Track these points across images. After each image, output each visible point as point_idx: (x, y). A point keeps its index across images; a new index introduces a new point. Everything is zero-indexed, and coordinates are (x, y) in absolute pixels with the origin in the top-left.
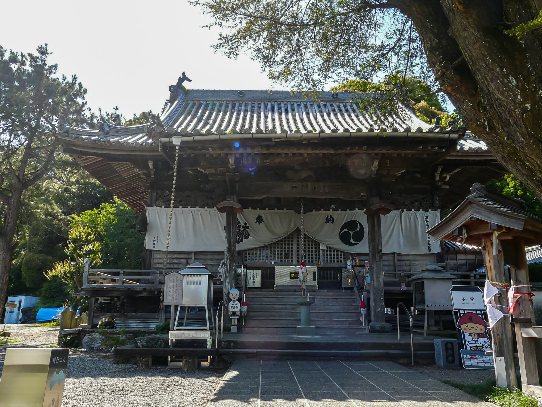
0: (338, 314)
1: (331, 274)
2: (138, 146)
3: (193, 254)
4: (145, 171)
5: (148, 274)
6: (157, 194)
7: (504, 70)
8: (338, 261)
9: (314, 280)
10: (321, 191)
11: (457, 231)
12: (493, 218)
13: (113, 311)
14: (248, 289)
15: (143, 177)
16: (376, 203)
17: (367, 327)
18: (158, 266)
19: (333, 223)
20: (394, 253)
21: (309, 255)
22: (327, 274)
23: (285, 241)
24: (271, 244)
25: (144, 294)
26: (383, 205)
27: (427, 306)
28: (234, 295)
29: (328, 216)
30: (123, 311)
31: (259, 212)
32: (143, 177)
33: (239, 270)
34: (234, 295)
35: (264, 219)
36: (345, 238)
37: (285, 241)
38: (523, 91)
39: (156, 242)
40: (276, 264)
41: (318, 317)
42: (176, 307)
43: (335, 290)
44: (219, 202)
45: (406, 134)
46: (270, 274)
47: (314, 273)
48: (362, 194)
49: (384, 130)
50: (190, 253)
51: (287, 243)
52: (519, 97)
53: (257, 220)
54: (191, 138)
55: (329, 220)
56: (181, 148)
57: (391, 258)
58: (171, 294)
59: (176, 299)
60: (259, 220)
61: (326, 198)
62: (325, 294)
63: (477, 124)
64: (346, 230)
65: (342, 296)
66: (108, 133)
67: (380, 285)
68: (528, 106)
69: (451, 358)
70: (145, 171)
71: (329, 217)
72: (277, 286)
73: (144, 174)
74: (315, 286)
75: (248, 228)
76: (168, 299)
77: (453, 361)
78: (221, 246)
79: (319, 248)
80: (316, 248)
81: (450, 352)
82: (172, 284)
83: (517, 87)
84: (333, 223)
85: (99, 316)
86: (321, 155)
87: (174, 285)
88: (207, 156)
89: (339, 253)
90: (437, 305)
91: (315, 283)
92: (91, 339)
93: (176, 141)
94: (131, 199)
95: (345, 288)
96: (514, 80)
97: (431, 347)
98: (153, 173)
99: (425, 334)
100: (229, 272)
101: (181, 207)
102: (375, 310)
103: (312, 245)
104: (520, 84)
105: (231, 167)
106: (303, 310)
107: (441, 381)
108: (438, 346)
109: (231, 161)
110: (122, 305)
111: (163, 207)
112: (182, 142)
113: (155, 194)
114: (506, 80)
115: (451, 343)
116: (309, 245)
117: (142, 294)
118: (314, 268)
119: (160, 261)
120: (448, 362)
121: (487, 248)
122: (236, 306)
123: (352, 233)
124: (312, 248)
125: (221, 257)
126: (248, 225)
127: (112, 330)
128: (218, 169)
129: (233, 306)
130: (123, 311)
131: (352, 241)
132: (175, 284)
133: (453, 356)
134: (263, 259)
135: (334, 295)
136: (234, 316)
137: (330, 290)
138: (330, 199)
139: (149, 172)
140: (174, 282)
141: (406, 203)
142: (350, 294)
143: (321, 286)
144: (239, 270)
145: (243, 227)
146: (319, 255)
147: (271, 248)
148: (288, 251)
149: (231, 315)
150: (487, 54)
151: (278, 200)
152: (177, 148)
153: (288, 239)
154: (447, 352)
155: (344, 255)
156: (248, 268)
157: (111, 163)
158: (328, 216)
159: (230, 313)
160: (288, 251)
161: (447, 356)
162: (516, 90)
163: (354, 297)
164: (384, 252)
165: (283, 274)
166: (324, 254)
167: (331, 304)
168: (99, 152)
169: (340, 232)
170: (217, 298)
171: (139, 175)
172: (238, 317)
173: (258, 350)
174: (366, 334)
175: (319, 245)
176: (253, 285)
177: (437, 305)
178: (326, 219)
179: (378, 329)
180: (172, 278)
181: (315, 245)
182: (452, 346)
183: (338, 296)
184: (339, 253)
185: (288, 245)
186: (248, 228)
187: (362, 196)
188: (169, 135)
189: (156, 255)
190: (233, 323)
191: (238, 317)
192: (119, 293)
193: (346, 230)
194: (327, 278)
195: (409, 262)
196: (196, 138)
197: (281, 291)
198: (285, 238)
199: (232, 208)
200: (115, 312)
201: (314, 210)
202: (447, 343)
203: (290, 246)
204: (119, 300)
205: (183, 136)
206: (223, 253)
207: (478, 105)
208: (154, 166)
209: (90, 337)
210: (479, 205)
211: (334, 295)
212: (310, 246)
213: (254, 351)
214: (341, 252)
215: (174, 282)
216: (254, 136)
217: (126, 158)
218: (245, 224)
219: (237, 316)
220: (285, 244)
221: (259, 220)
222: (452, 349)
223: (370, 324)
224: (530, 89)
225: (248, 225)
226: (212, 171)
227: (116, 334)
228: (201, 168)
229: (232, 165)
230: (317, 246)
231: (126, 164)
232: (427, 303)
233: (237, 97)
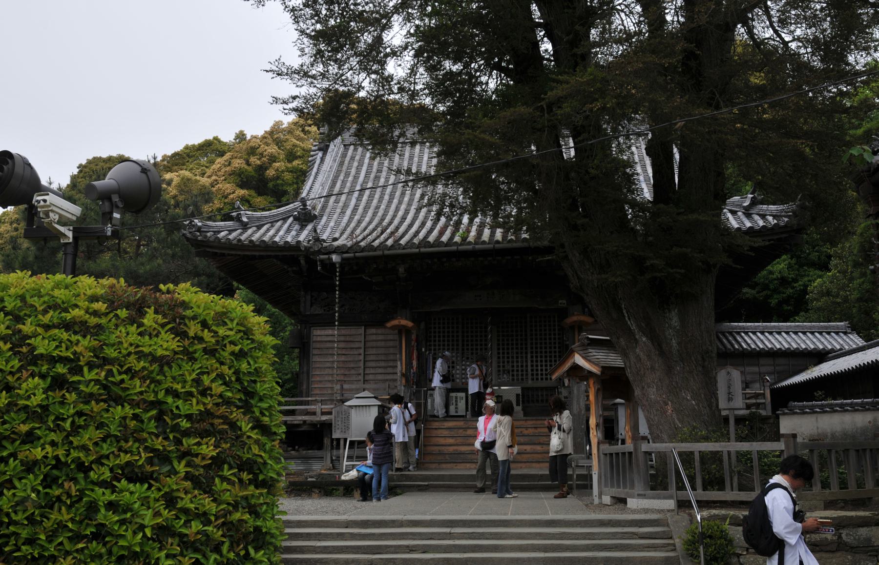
4: (295, 268)
6: (312, 297)
25: (304, 428)
47: (518, 395)
56: (341, 264)
70: (295, 268)
93: (335, 258)
109: (401, 270)
112: (343, 259)
113: (309, 297)
194: (538, 401)
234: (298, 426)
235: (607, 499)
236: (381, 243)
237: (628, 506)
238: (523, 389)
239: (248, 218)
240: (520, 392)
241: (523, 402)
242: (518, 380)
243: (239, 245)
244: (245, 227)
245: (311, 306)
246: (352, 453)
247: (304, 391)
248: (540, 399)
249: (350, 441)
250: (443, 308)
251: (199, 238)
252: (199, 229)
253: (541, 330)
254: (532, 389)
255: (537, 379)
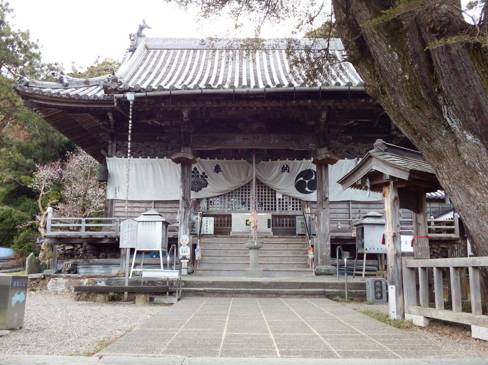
0: (288, 258)
1: (286, 221)
2: (96, 99)
3: (153, 203)
4: (105, 123)
5: (110, 222)
6: (117, 144)
7: (389, 46)
8: (297, 209)
9: (269, 227)
10: (272, 142)
11: (360, 181)
12: (388, 170)
13: (76, 257)
14: (202, 236)
15: (103, 128)
16: (323, 153)
17: (314, 270)
18: (119, 214)
19: (288, 172)
20: (349, 201)
21: (265, 203)
22: (283, 221)
23: (242, 190)
24: (229, 193)
25: (106, 241)
26: (328, 156)
27: (366, 249)
28: (184, 240)
29: (284, 166)
30: (85, 257)
31: (216, 161)
32: (103, 128)
33: (194, 218)
34: (184, 240)
35: (221, 167)
36: (300, 187)
37: (242, 190)
38: (403, 64)
39: (117, 192)
40: (232, 211)
41: (268, 261)
42: (132, 250)
43: (286, 236)
44: (173, 154)
45: (347, 88)
46: (228, 221)
47: (269, 220)
48: (311, 145)
49: (327, 85)
50: (150, 202)
51: (244, 191)
52: (400, 69)
53: (215, 170)
54: (143, 94)
55: (285, 169)
56: (135, 102)
57: (345, 206)
58: (126, 238)
59: (131, 243)
60: (217, 169)
61: (272, 149)
62: (277, 239)
63: (373, 89)
64: (301, 179)
65: (294, 241)
66: (67, 85)
67: (326, 231)
68: (407, 77)
69: (379, 295)
70: (105, 123)
71: (285, 166)
72: (233, 233)
73: (104, 125)
74: (269, 233)
75: (206, 177)
76: (124, 244)
77: (381, 297)
78: (176, 194)
79: (275, 196)
80: (272, 196)
81: (378, 289)
82: (127, 230)
83: (399, 61)
84: (288, 172)
85: (63, 262)
86: (269, 108)
87: (129, 231)
88: (162, 109)
89: (295, 201)
90: (376, 249)
91: (270, 229)
92: (56, 283)
93: (130, 97)
94: (93, 149)
95: (299, 235)
96: (397, 55)
97: (363, 286)
98: (112, 124)
99: (363, 275)
100: (184, 219)
101: (140, 157)
102: (321, 254)
103: (268, 193)
104: (401, 59)
105: (185, 120)
106: (252, 253)
107: (364, 313)
108: (368, 284)
109: (185, 114)
110: (85, 252)
111: (123, 157)
112: (136, 98)
113: (115, 145)
114: (390, 55)
115: (381, 282)
116: (265, 193)
117: (103, 241)
118: (269, 215)
119: (121, 209)
120: (377, 298)
121: (386, 195)
122: (186, 251)
123: (307, 181)
124: (269, 196)
125: (175, 205)
126: (206, 174)
127: (76, 275)
128: (174, 122)
129: (183, 250)
130: (85, 257)
131: (307, 189)
132: (130, 229)
133: (381, 292)
134: (218, 208)
135: (285, 241)
136: (184, 259)
137: (281, 236)
138: (268, 149)
139: (109, 124)
140: (129, 227)
141: (362, 152)
142: (301, 240)
143: (275, 232)
144: (194, 218)
145: (201, 176)
146: (275, 203)
147: (229, 196)
148: (246, 199)
149: (182, 259)
150: (376, 32)
151: (236, 151)
152: (131, 103)
153: (247, 187)
154: (375, 289)
155: (300, 203)
156: (203, 216)
157: (71, 114)
158: (284, 166)
159: (181, 257)
160: (246, 199)
161: (376, 293)
162: (398, 63)
163: (304, 242)
164: (331, 199)
165: (239, 221)
166: (279, 203)
167: (283, 249)
168: (59, 104)
169: (296, 180)
170: (172, 243)
171: (99, 125)
172: (188, 261)
173: (206, 289)
174: (312, 277)
175: (275, 193)
176: (207, 232)
177: (376, 249)
178: (282, 168)
179: (324, 271)
180: (127, 224)
181: (272, 193)
182: (381, 284)
183: (289, 241)
184: (295, 201)
185: (242, 193)
186: (206, 177)
187: (311, 146)
188: (124, 91)
189: (117, 204)
190: (183, 266)
191: (188, 261)
192: (81, 240)
193: (301, 179)
194: (279, 225)
195: (358, 210)
196: (148, 94)
197: (236, 237)
198: (242, 187)
199: (187, 159)
200: (77, 258)
201: (270, 160)
202: (376, 282)
203: (247, 195)
204: (82, 247)
205: (136, 92)
206: (177, 202)
207: (374, 74)
208: (114, 118)
209: (54, 281)
210: (378, 159)
211: (285, 241)
212: (267, 195)
213: (202, 289)
214: (297, 199)
215: (129, 227)
216: (204, 91)
217: (88, 110)
218: (204, 173)
219: (187, 259)
220: (242, 193)
221: (217, 169)
222: (381, 287)
223: (317, 267)
224: (408, 63)
225: (206, 174)
226: (168, 123)
227: (80, 278)
228: (157, 121)
229: (186, 118)
230: (273, 195)
231: (86, 116)
232: (366, 246)
233: (198, 45)
234: (101, 239)
235: (420, 321)
236: (171, 86)
237: (474, 335)
238: (273, 216)
239: (69, 81)
240: (270, 218)
241: (272, 225)
242: (269, 209)
243: (58, 98)
244: (66, 86)
245: (116, 152)
246: (138, 262)
247: (109, 214)
248: (285, 223)
249: (137, 251)
250: (218, 148)
251: (27, 91)
252: (27, 85)
253: (262, 193)
254: (279, 216)
255: (283, 209)
